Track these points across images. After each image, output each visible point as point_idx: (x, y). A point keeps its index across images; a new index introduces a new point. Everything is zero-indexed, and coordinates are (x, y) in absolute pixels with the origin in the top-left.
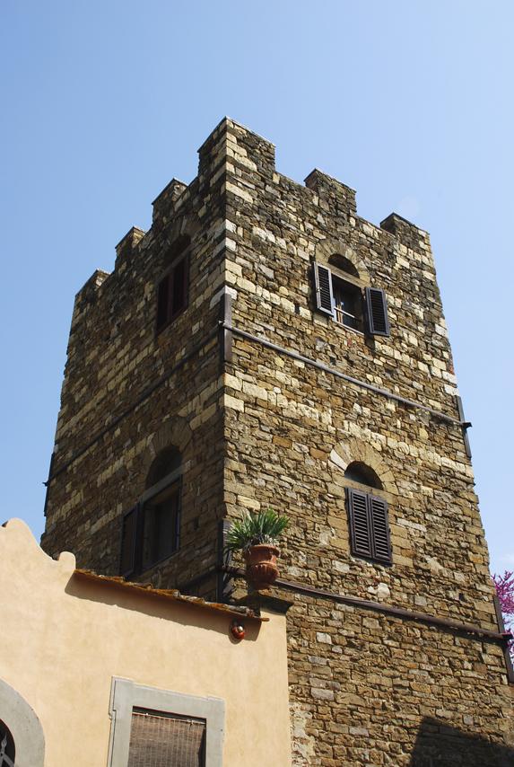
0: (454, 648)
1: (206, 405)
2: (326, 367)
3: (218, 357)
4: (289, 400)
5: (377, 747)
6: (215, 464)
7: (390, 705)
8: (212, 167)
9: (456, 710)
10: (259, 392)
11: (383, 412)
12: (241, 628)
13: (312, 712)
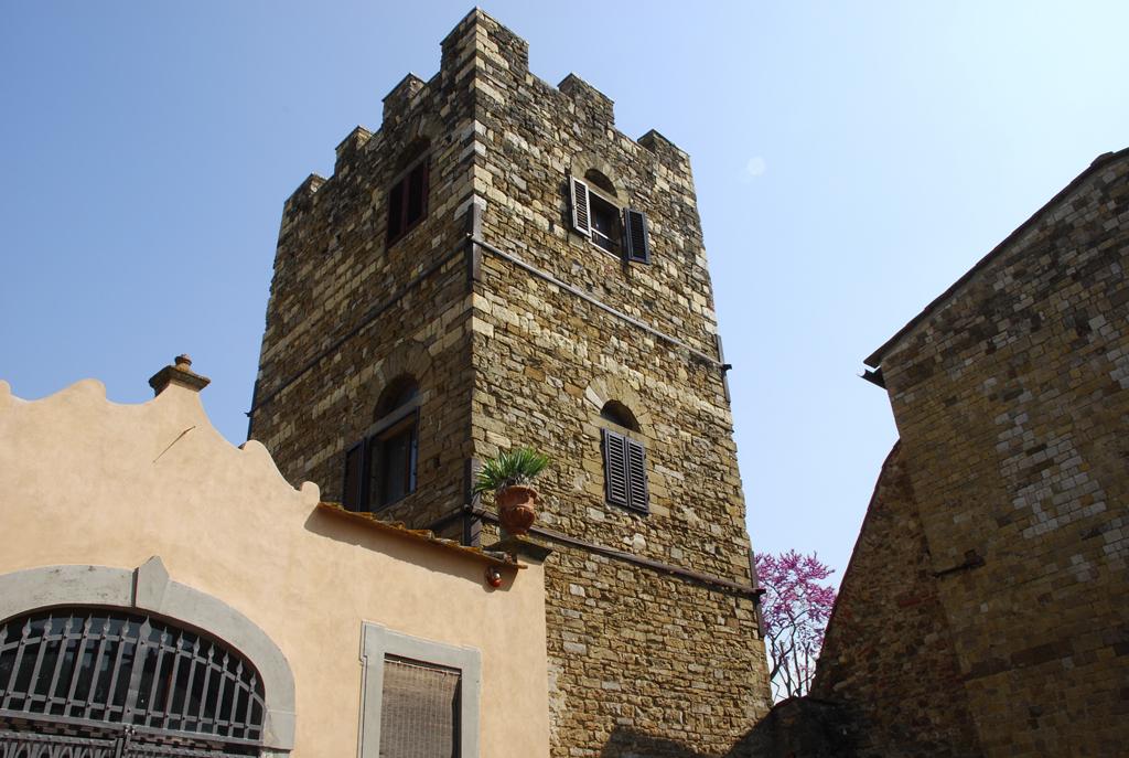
0: (708, 603)
1: (449, 328)
2: (582, 294)
3: (465, 274)
4: (542, 327)
5: (629, 702)
6: (460, 395)
7: (643, 660)
8: (459, 62)
9: (708, 664)
10: (510, 316)
11: (641, 347)
12: (498, 575)
13: (564, 666)
